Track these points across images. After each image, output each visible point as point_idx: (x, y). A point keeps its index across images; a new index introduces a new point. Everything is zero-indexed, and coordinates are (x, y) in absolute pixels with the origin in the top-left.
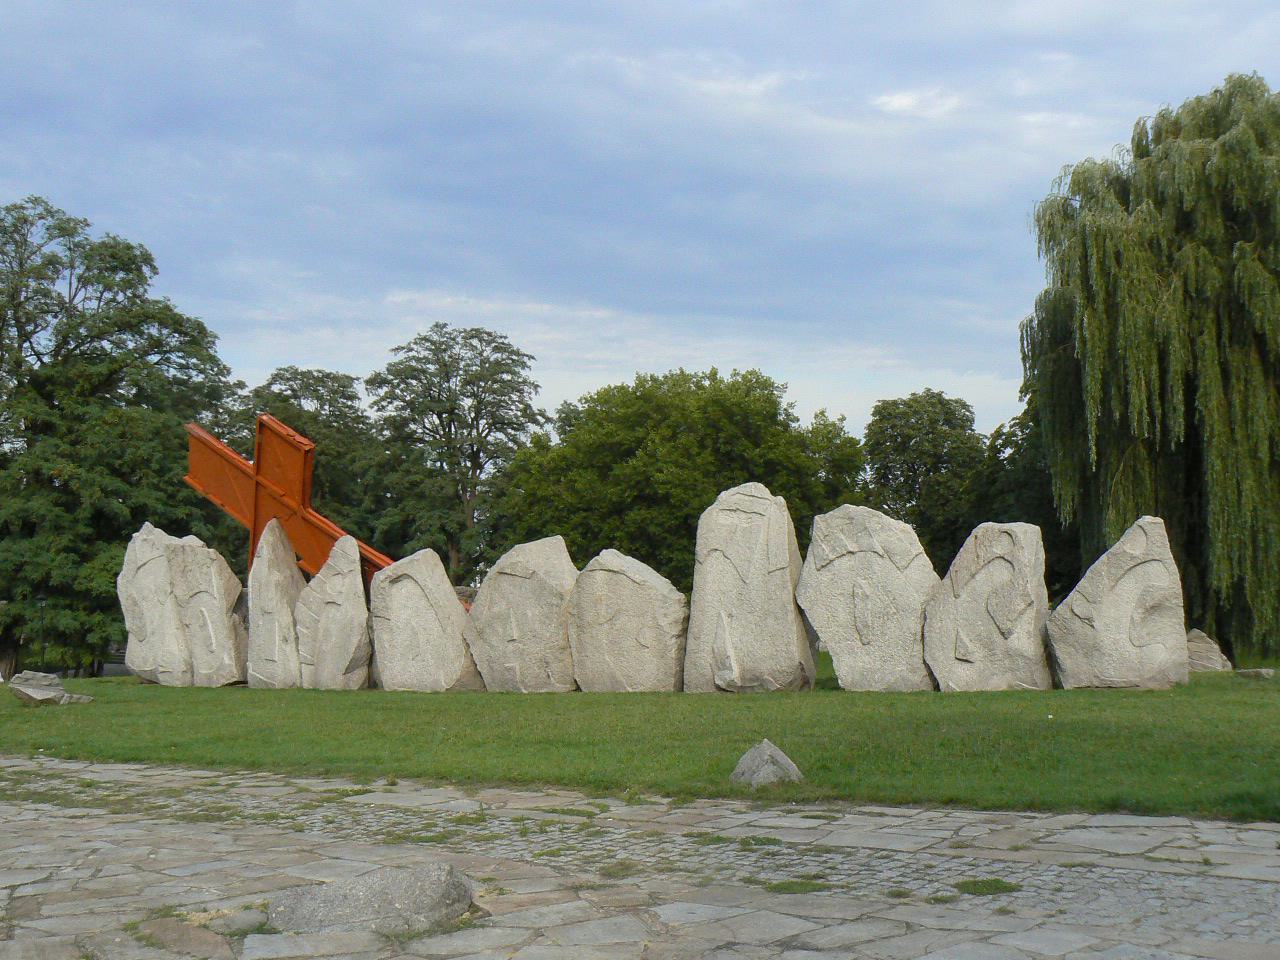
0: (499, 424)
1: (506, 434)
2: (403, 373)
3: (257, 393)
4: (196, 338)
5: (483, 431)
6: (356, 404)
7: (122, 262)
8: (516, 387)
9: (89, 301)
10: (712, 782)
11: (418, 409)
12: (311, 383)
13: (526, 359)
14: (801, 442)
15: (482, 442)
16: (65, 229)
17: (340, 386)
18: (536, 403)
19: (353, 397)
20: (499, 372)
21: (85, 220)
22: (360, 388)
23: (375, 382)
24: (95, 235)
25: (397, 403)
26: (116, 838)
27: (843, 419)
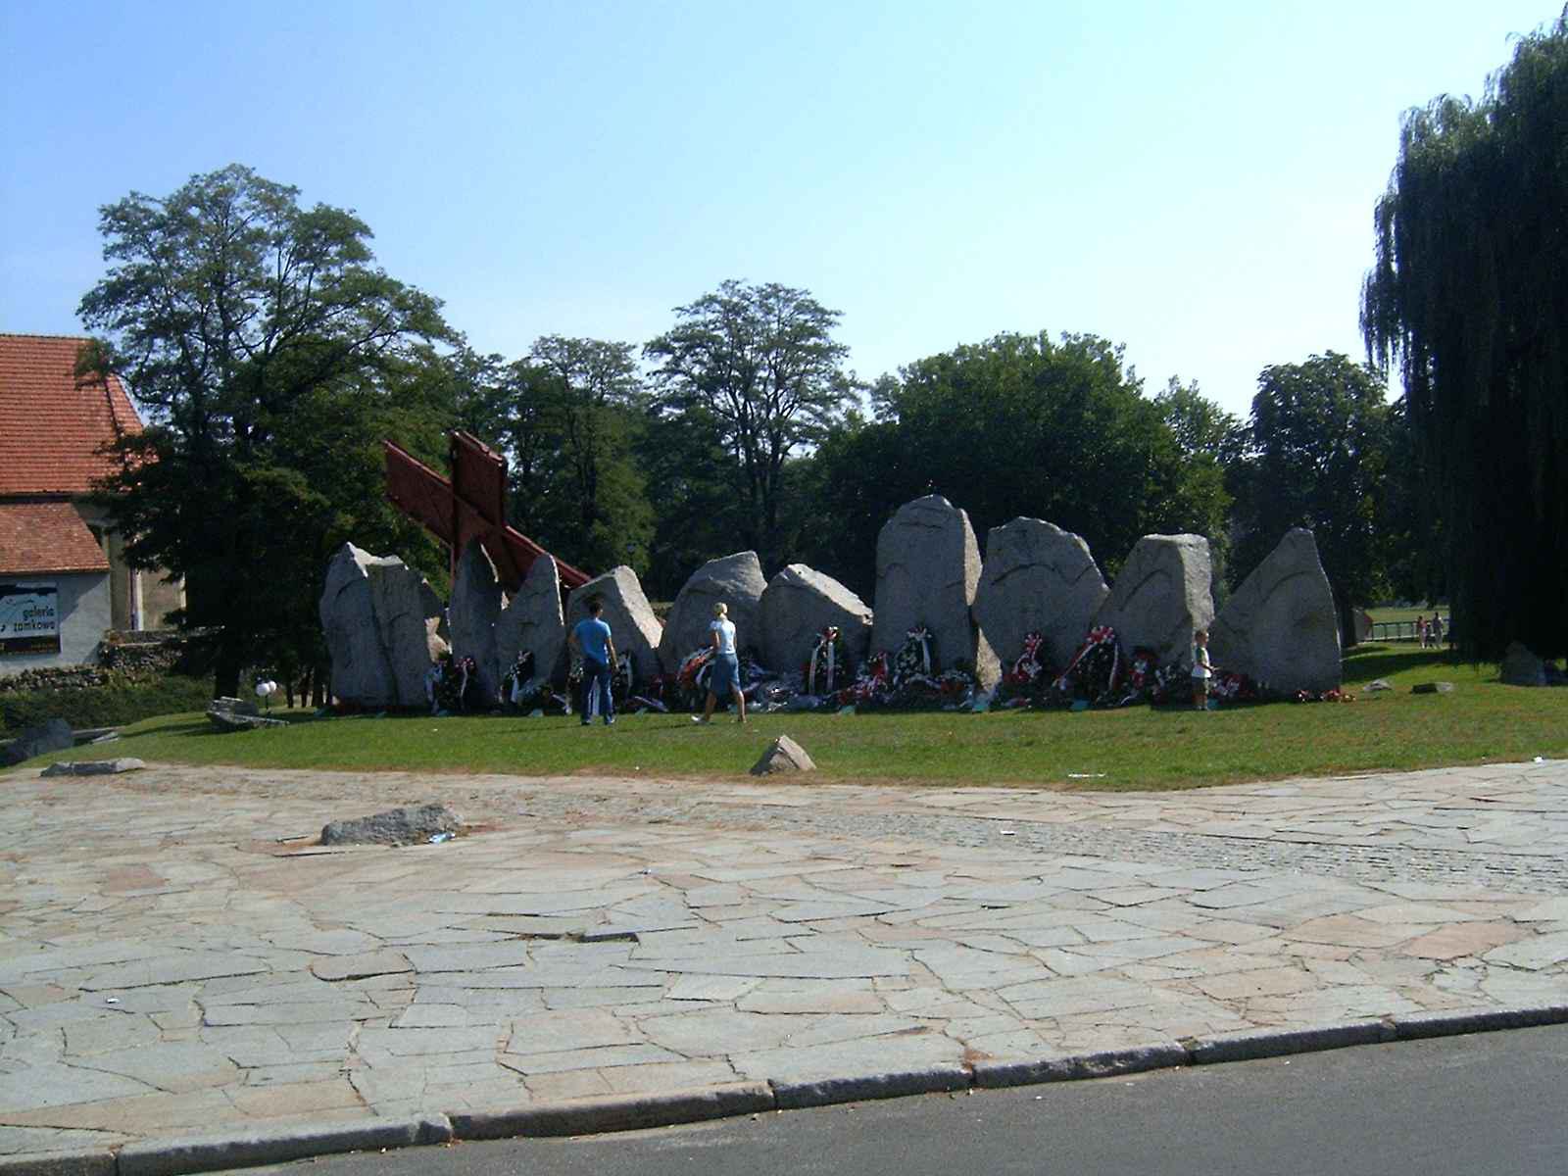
0: (801, 398)
1: (813, 412)
2: (690, 340)
3: (517, 366)
4: (423, 315)
5: (784, 411)
6: (635, 375)
7: (330, 233)
8: (825, 352)
9: (305, 282)
10: (366, 692)
11: (711, 384)
12: (575, 351)
13: (833, 317)
14: (1151, 413)
15: (781, 420)
16: (274, 198)
17: (615, 357)
18: (845, 367)
19: (629, 368)
20: (801, 335)
21: (294, 187)
22: (635, 355)
23: (659, 347)
24: (306, 205)
25: (679, 378)
26: (870, 840)
27: (1195, 382)
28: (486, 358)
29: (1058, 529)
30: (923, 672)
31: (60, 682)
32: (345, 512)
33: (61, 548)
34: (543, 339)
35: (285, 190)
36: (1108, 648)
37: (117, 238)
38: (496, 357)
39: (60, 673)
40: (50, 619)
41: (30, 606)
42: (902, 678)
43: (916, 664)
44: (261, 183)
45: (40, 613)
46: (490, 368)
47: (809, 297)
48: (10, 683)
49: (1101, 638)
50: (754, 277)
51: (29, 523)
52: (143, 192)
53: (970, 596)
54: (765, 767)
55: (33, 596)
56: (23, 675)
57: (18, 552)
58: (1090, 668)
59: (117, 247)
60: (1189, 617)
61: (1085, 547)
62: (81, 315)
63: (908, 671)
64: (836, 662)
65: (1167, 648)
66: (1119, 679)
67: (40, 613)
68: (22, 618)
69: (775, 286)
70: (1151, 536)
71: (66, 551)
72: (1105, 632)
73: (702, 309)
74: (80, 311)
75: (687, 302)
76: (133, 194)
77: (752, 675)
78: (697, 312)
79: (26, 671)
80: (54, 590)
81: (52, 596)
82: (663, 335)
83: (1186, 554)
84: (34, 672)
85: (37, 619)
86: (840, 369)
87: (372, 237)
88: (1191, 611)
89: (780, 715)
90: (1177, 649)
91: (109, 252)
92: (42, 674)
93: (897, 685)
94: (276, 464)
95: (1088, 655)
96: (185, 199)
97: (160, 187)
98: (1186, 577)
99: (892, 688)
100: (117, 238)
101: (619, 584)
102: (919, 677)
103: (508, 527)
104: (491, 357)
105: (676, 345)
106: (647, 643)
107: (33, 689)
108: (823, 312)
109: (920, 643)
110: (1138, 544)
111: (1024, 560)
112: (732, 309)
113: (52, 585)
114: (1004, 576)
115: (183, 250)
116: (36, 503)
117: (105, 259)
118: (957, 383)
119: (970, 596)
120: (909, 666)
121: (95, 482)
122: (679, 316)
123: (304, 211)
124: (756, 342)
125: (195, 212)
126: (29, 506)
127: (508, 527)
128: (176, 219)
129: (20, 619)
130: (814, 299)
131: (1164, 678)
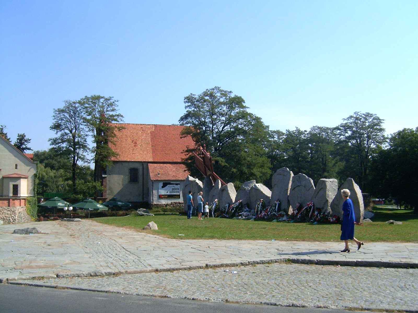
8: (381, 130)
13: (382, 121)
16: (224, 94)
20: (376, 125)
28: (303, 131)
29: (307, 176)
30: (275, 212)
31: (179, 205)
32: (234, 168)
33: (182, 174)
34: (313, 126)
35: (228, 92)
36: (310, 208)
37: (187, 104)
38: (306, 131)
39: (180, 203)
40: (178, 191)
41: (174, 188)
42: (271, 213)
43: (274, 209)
44: (221, 91)
45: (176, 189)
46: (304, 134)
47: (376, 116)
48: (168, 205)
49: (309, 205)
50: (363, 111)
51: (177, 169)
52: (193, 93)
53: (288, 194)
54: (144, 229)
55: (175, 185)
56: (171, 203)
57: (172, 175)
58: (305, 212)
59: (188, 106)
60: (327, 201)
61: (312, 181)
62: (179, 122)
63: (272, 211)
64: (261, 208)
65: (323, 208)
66: (311, 216)
67: (176, 189)
68: (172, 190)
69: (368, 113)
70: (322, 179)
71: (183, 175)
72: (311, 203)
73: (349, 119)
74: (179, 121)
75: (346, 117)
76: (191, 94)
77: (245, 210)
78: (348, 120)
79: (172, 202)
80: (179, 184)
81: (179, 185)
82: (338, 126)
83: (328, 184)
84: (174, 203)
85: (175, 191)
86: (384, 134)
87: (245, 103)
88: (328, 199)
89: (243, 220)
90: (325, 209)
91: (186, 107)
92: (176, 203)
93: (269, 214)
94: (218, 156)
95: (305, 209)
96: (205, 94)
97: (197, 92)
98: (327, 190)
99: (268, 215)
100: (187, 104)
101: (228, 187)
102: (274, 213)
103: (214, 173)
104: (305, 131)
105: (342, 128)
106: (232, 201)
107: (173, 207)
108: (380, 120)
109: (276, 204)
110: (319, 181)
111: (299, 185)
112: (357, 119)
113: (179, 183)
114: (295, 188)
115: (202, 106)
116: (179, 164)
117: (186, 109)
118: (403, 138)
119: (288, 194)
120: (273, 210)
121: (182, 159)
122: (344, 121)
123: (232, 97)
124: (365, 126)
125: (207, 98)
126: (177, 165)
127: (214, 173)
128: (202, 100)
129: (171, 190)
130: (378, 116)
131: (320, 216)
